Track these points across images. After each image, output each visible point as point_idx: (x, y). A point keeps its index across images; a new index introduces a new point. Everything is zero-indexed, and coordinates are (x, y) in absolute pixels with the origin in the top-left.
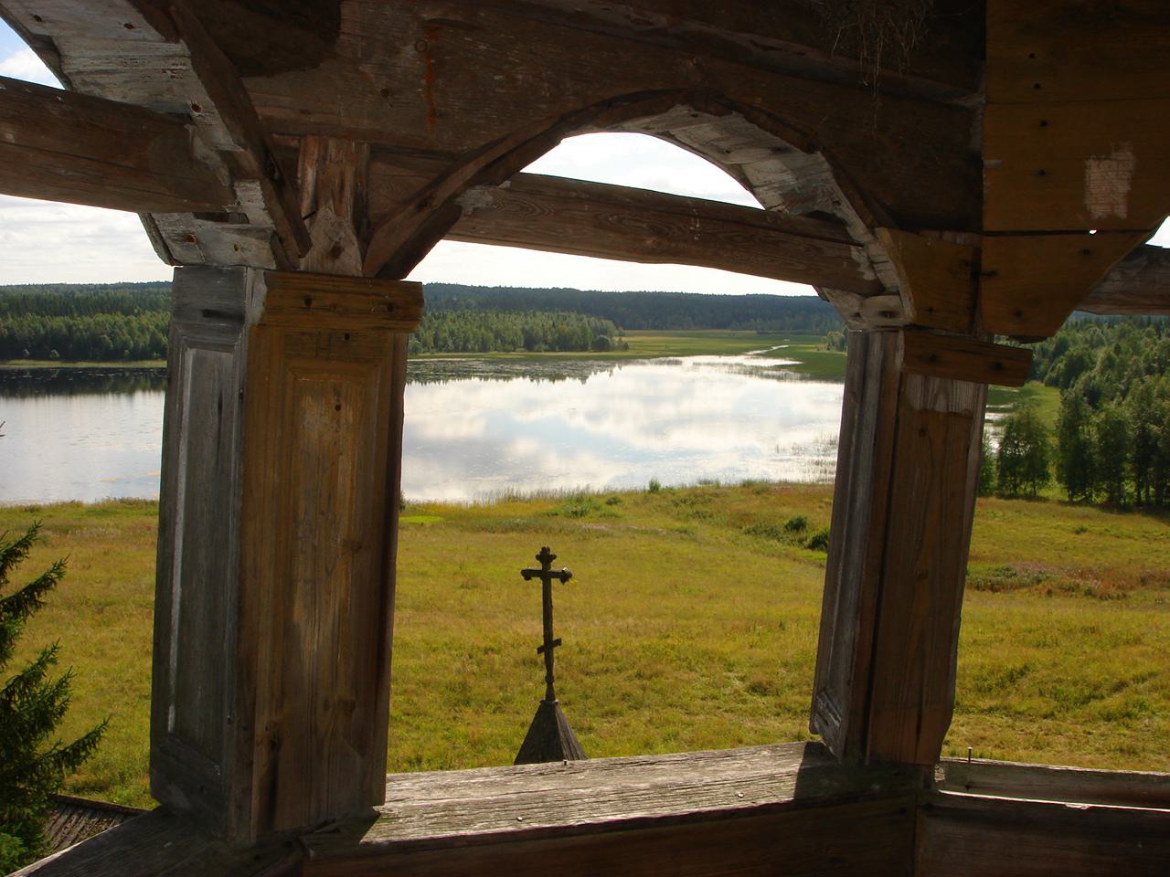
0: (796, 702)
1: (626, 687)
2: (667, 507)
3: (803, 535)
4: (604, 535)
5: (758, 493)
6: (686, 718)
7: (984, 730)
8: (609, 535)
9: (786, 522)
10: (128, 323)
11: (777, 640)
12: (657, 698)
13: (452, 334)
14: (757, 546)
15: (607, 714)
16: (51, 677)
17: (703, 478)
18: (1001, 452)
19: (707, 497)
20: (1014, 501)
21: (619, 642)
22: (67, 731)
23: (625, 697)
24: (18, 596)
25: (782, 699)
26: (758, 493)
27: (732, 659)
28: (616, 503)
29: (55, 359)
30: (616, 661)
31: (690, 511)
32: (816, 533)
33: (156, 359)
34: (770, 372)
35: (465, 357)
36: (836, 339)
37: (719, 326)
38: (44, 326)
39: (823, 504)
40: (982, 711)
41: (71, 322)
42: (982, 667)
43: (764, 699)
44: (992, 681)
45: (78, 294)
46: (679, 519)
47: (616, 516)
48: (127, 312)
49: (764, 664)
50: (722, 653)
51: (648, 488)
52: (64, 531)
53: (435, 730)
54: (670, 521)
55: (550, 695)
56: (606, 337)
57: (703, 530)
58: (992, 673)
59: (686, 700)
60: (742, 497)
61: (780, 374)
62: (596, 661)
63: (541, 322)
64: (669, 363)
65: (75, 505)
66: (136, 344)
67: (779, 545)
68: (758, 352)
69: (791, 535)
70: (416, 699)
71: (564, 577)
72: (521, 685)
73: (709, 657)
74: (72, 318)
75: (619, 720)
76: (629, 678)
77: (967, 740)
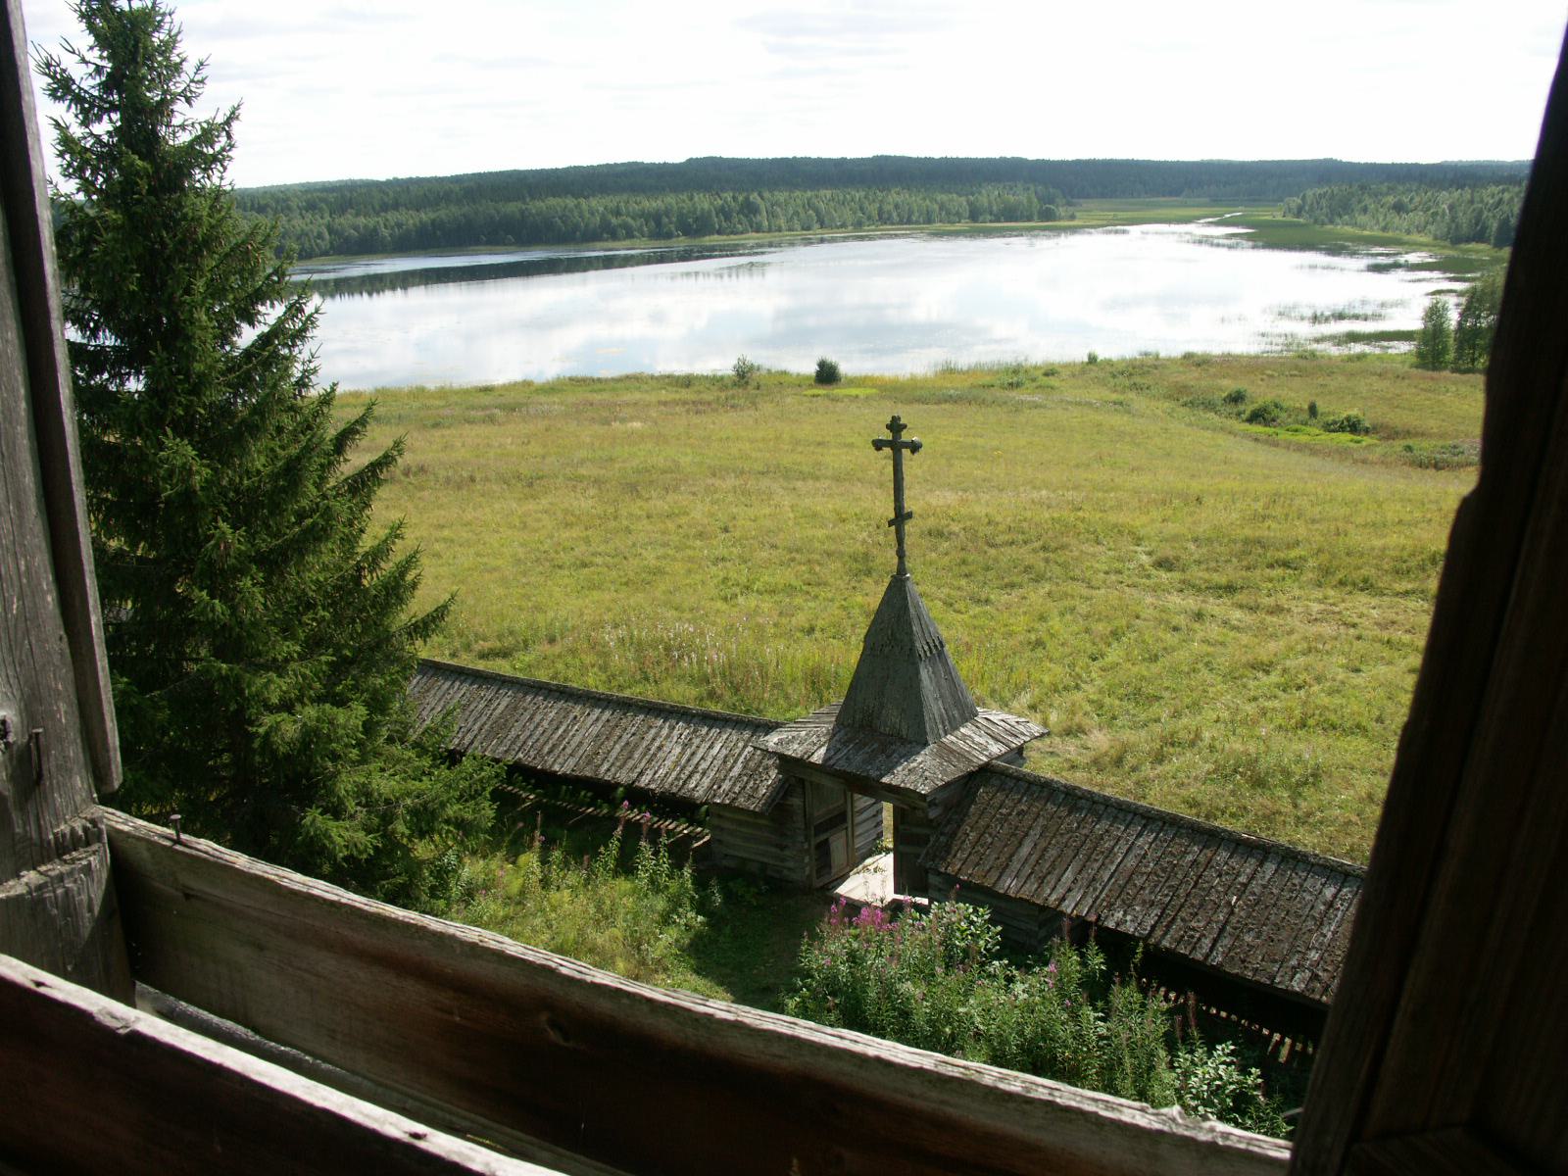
0: (1201, 578)
1: (1030, 559)
2: (1103, 379)
3: (1241, 407)
4: (1036, 406)
5: (1199, 365)
6: (1085, 592)
7: (1397, 613)
8: (1041, 407)
9: (1224, 395)
10: (578, 206)
11: (1191, 514)
12: (1057, 570)
13: (897, 206)
14: (1193, 419)
15: (1006, 586)
16: (399, 552)
17: (1143, 349)
18: (1460, 323)
19: (1146, 369)
20: (1471, 375)
21: (1029, 514)
22: (418, 606)
23: (1028, 569)
24: (361, 474)
25: (1187, 576)
26: (1199, 365)
27: (1142, 533)
28: (1053, 374)
30: (1023, 533)
31: (1127, 383)
32: (1256, 406)
33: (607, 240)
34: (1221, 241)
35: (906, 229)
36: (1293, 205)
37: (1171, 194)
38: (498, 213)
39: (1264, 377)
40: (1397, 594)
41: (524, 207)
42: (1404, 548)
43: (1169, 575)
44: (1413, 563)
46: (1116, 391)
47: (1052, 388)
49: (1175, 538)
50: (1132, 526)
51: (1086, 360)
52: (511, 409)
53: (832, 600)
54: (1107, 393)
55: (902, 570)
56: (1052, 207)
57: (1138, 401)
58: (1413, 555)
59: (1088, 574)
60: (1181, 369)
61: (1232, 243)
62: (1002, 533)
64: (1116, 232)
65: (527, 384)
66: (587, 226)
67: (1216, 418)
68: (1210, 220)
69: (1231, 408)
70: (817, 569)
71: (915, 447)
72: (924, 555)
73: (1119, 530)
74: (525, 203)
75: (1016, 592)
76: (1034, 551)
77: (1376, 624)
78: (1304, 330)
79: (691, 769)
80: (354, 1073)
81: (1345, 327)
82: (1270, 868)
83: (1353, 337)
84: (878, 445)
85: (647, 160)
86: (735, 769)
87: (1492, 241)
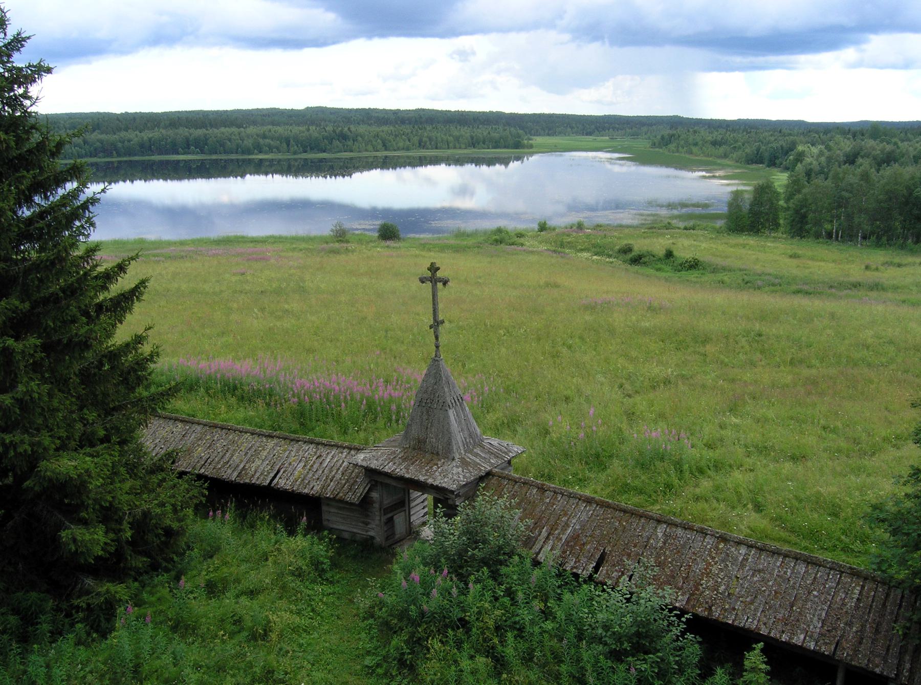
16: (146, 349)
29: (193, 153)
37: (587, 134)
45: (211, 117)
48: (239, 126)
63: (482, 132)
74: (207, 130)
78: (664, 212)
80: (639, 210)
84: (422, 281)
85: (282, 107)
87: (766, 163)
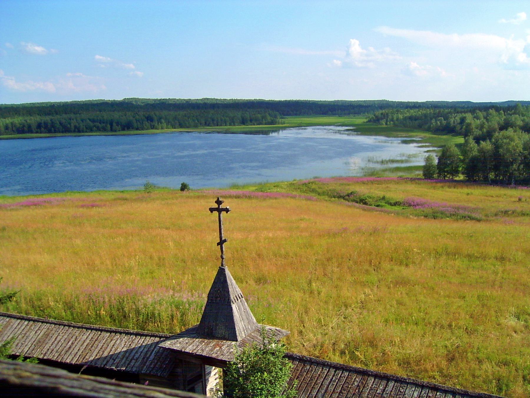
71: (227, 210)
74: (53, 116)
79: (131, 358)
81: (395, 165)
82: (391, 384)
83: (397, 169)
86: (151, 357)
